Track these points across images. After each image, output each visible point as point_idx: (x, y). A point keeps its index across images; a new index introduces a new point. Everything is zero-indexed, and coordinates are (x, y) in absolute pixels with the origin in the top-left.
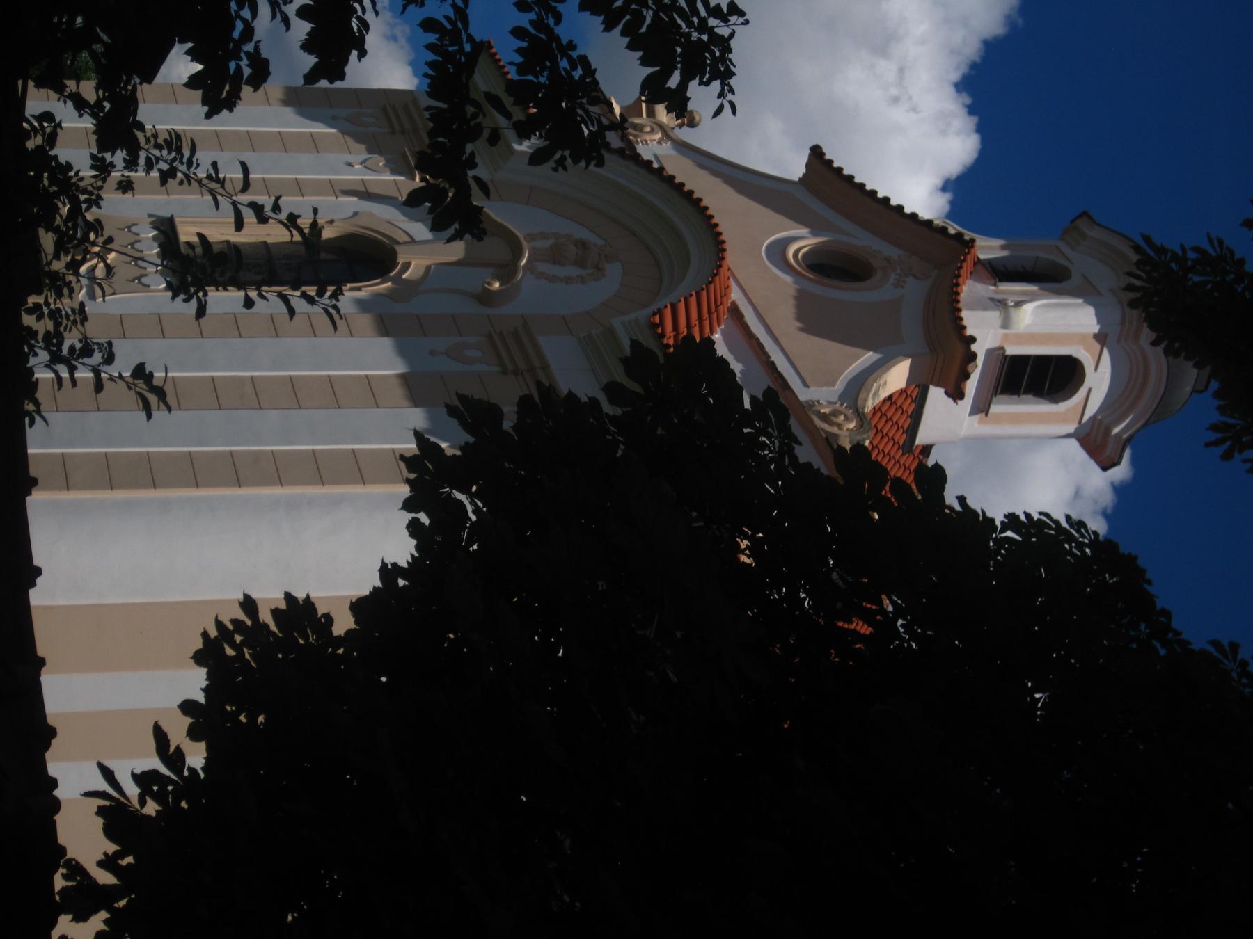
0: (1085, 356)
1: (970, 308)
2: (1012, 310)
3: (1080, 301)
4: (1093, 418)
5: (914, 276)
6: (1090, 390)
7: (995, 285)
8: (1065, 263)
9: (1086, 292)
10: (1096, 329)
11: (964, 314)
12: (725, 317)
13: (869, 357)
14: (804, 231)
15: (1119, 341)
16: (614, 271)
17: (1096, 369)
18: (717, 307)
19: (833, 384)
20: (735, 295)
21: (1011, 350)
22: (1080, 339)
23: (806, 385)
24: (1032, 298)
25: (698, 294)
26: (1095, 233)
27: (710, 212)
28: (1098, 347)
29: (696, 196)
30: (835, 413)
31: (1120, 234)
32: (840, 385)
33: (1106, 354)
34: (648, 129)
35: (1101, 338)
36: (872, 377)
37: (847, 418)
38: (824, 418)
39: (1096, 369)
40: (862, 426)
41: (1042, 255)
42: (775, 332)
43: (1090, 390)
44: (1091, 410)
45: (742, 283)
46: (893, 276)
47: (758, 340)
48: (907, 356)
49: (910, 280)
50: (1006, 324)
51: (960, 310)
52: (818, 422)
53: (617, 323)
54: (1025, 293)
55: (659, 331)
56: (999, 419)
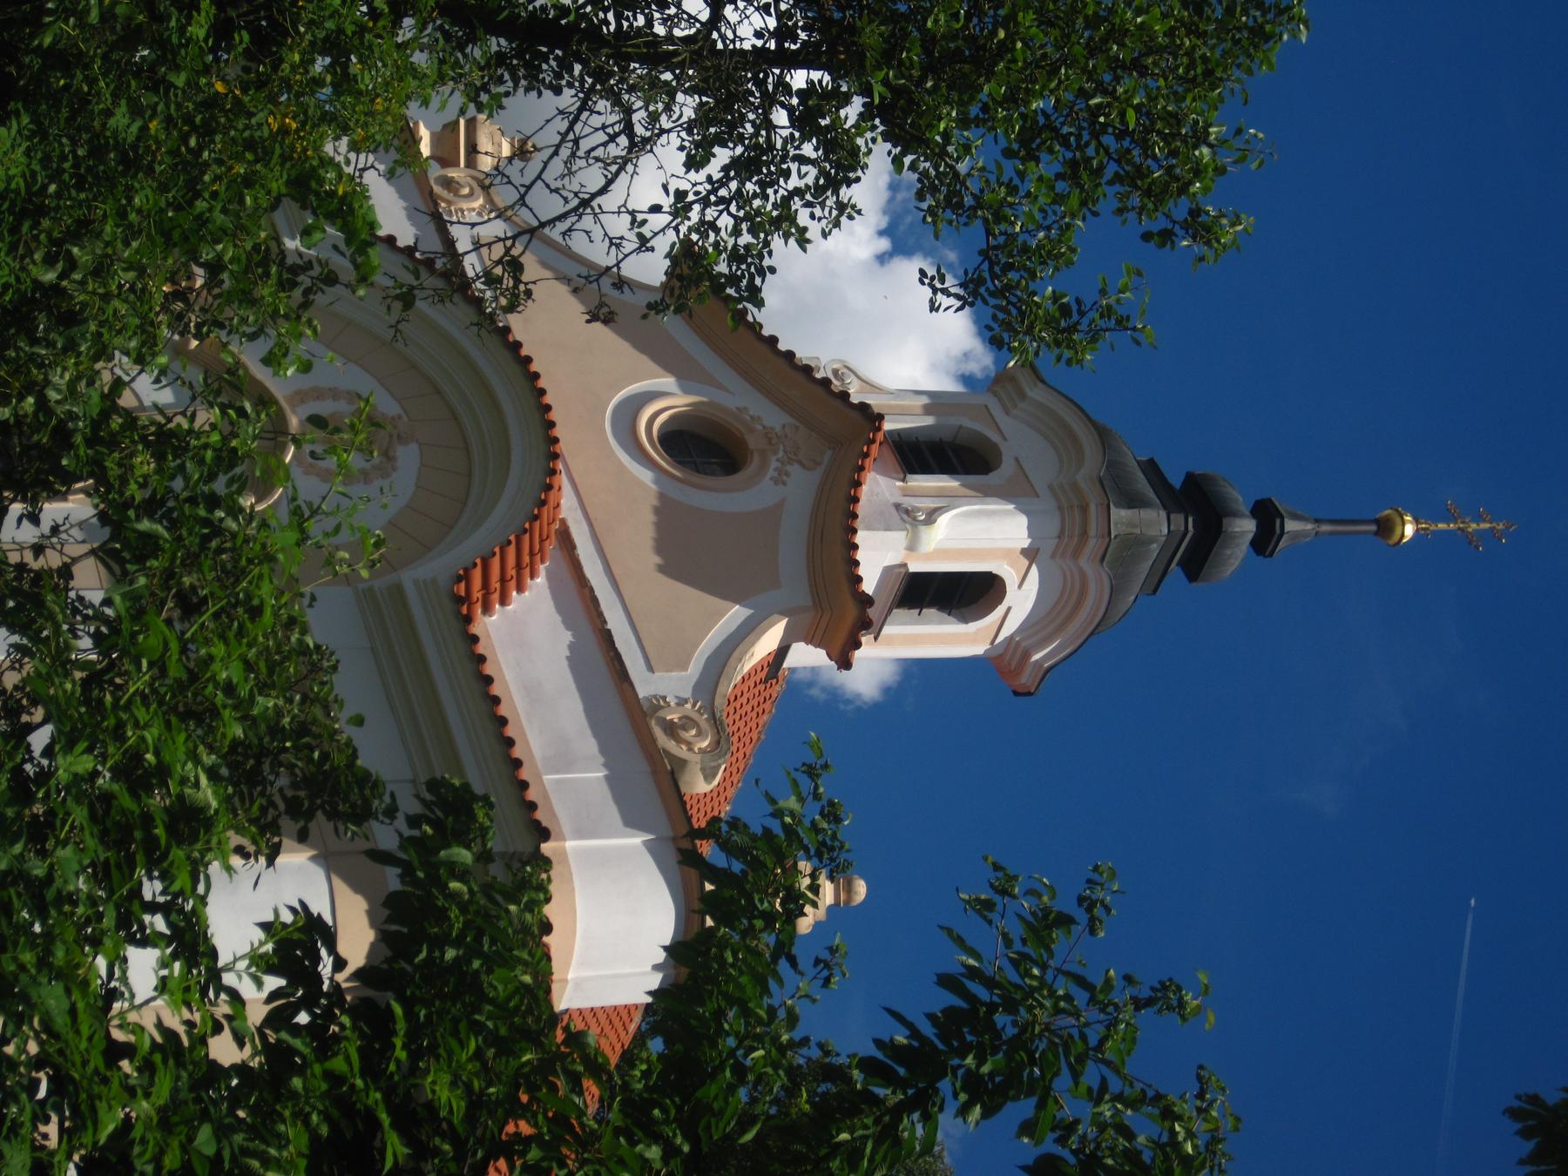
0: (1008, 572)
1: (869, 528)
2: (922, 528)
3: (1011, 507)
4: (1010, 639)
5: (800, 463)
6: (1009, 609)
7: (903, 480)
8: (994, 437)
9: (1017, 492)
10: (1026, 543)
11: (861, 538)
12: (551, 546)
13: (736, 614)
14: (667, 382)
15: (1053, 556)
16: (408, 457)
17: (1020, 586)
18: (542, 541)
19: (683, 666)
20: (568, 506)
21: (915, 567)
22: (1006, 554)
23: (651, 669)
24: (949, 501)
25: (518, 539)
26: (1037, 393)
27: (542, 383)
28: (1027, 563)
29: (524, 352)
30: (687, 722)
31: (1067, 397)
32: (695, 668)
33: (1034, 570)
34: (466, 191)
35: (1030, 554)
36: (736, 654)
37: (699, 734)
38: (671, 729)
39: (1020, 586)
40: (718, 742)
41: (967, 423)
42: (616, 572)
43: (1009, 609)
44: (1006, 632)
45: (577, 480)
46: (774, 464)
47: (592, 590)
48: (783, 613)
49: (795, 469)
50: (912, 547)
51: (855, 531)
52: (658, 732)
53: (408, 578)
54: (939, 494)
55: (464, 610)
56: (891, 640)
